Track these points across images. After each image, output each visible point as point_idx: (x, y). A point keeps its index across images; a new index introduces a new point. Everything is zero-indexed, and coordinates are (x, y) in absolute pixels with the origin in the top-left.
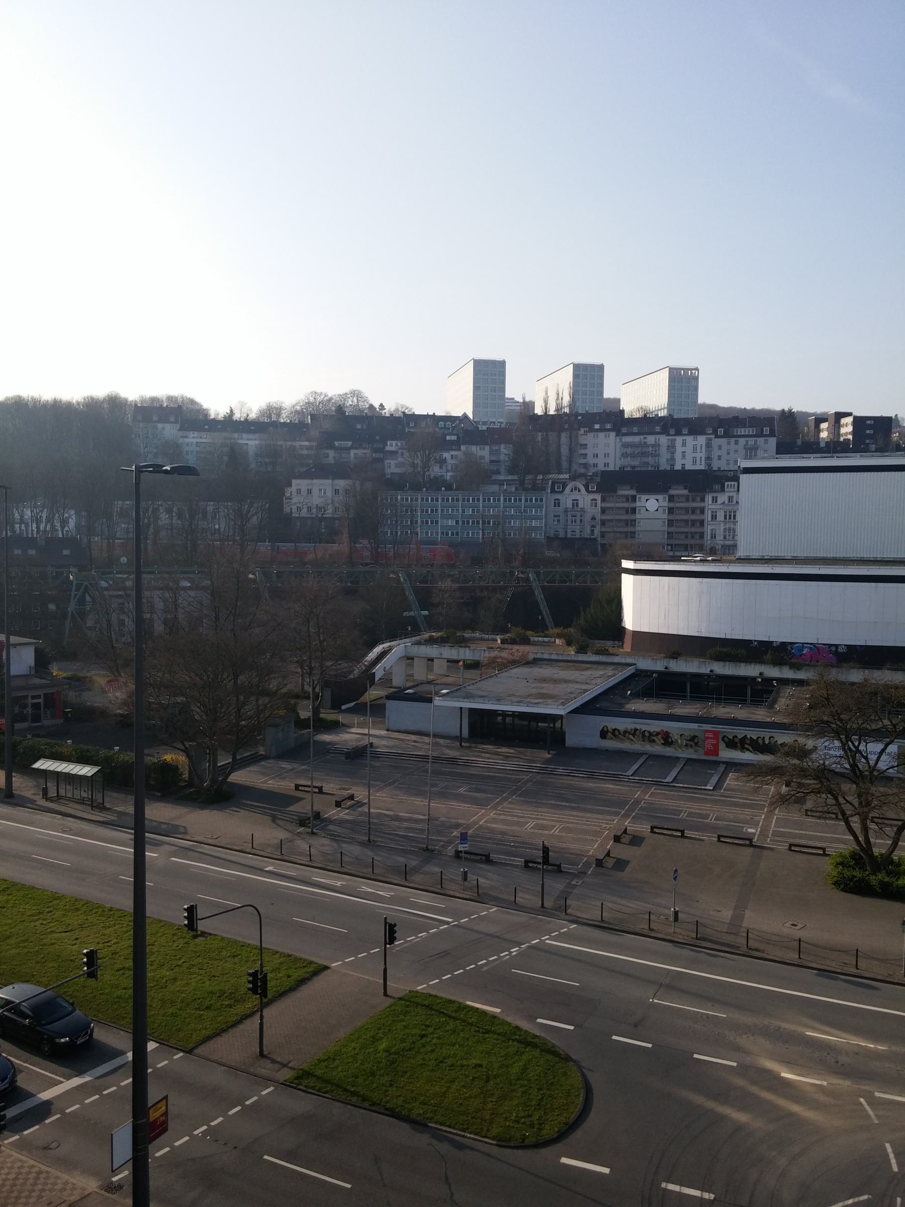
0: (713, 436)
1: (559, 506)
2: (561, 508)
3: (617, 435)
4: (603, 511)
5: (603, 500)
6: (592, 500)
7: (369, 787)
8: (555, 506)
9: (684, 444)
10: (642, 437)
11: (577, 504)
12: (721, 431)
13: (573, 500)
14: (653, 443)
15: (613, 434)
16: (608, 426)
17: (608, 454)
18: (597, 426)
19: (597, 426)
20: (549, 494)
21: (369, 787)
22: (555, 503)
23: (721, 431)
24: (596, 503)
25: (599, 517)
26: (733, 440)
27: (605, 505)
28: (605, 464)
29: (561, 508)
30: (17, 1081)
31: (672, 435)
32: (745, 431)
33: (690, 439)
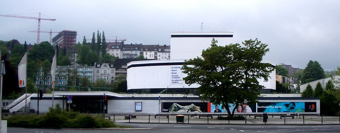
0: (157, 52)
1: (99, 73)
2: (100, 74)
3: (121, 50)
4: (116, 74)
5: (116, 70)
6: (112, 70)
7: (114, 116)
8: (97, 73)
9: (146, 54)
10: (130, 51)
11: (106, 72)
12: (160, 50)
13: (105, 70)
14: (135, 54)
15: (119, 50)
16: (118, 47)
17: (118, 54)
18: (113, 47)
19: (113, 47)
20: (95, 68)
21: (114, 116)
22: (97, 71)
23: (160, 50)
24: (113, 72)
25: (114, 76)
26: (164, 53)
27: (117, 72)
28: (117, 54)
29: (100, 74)
30: (204, 54)
31: (142, 51)
32: (168, 50)
33: (149, 53)
